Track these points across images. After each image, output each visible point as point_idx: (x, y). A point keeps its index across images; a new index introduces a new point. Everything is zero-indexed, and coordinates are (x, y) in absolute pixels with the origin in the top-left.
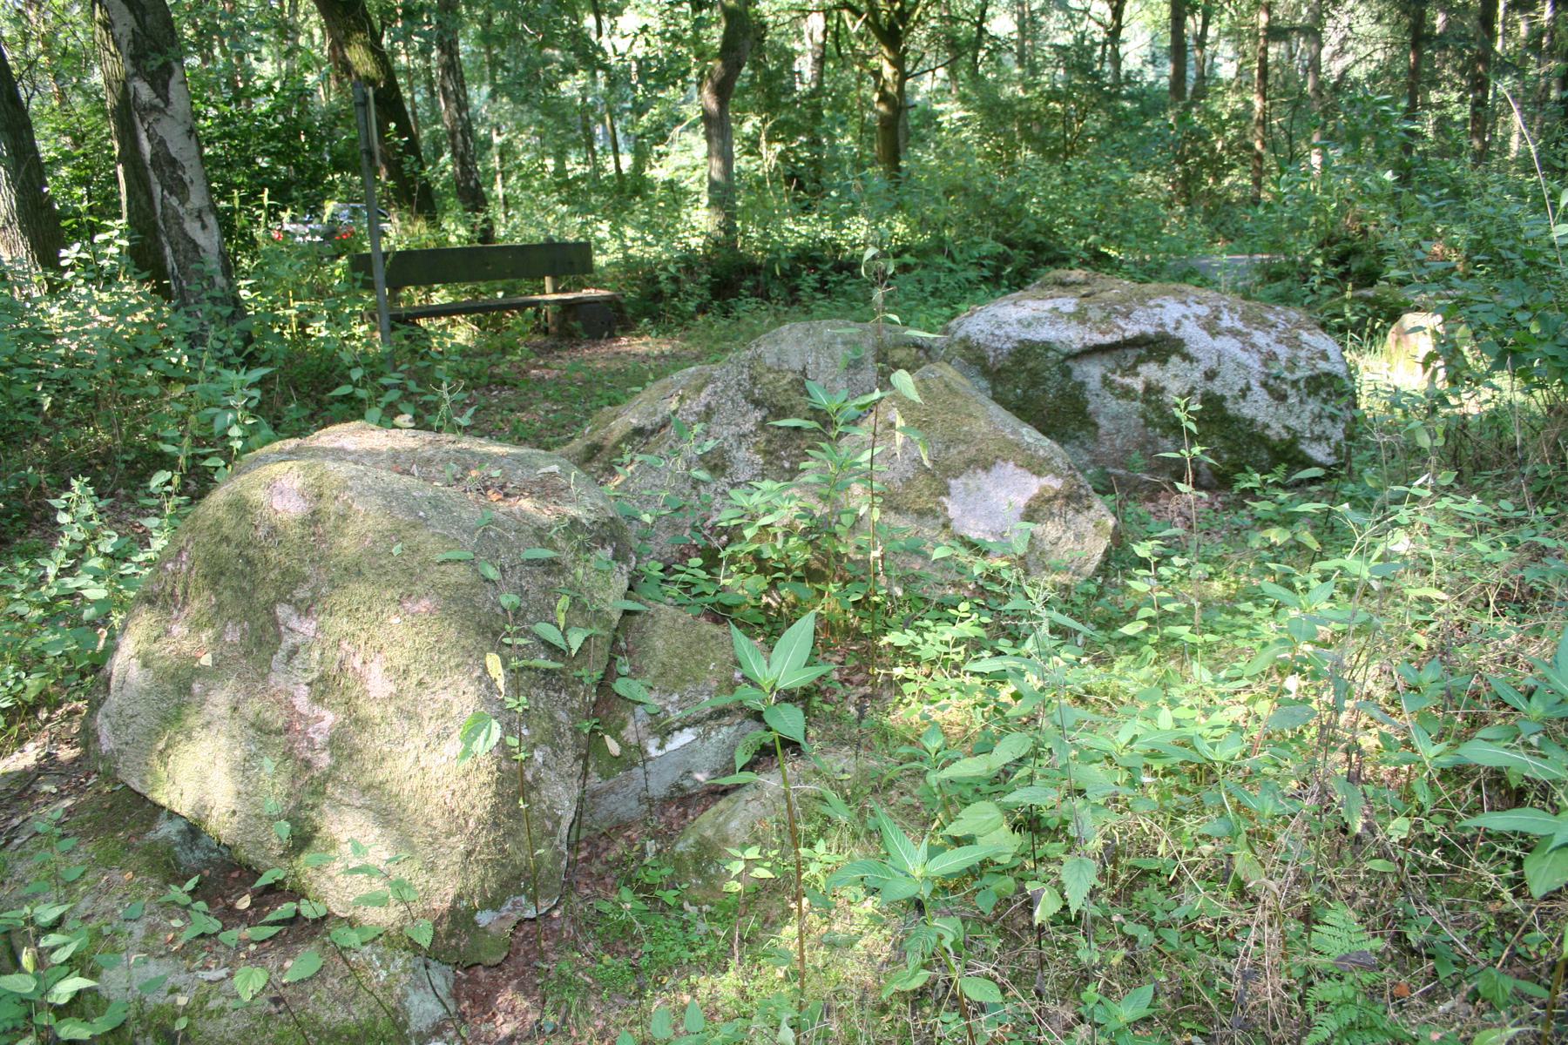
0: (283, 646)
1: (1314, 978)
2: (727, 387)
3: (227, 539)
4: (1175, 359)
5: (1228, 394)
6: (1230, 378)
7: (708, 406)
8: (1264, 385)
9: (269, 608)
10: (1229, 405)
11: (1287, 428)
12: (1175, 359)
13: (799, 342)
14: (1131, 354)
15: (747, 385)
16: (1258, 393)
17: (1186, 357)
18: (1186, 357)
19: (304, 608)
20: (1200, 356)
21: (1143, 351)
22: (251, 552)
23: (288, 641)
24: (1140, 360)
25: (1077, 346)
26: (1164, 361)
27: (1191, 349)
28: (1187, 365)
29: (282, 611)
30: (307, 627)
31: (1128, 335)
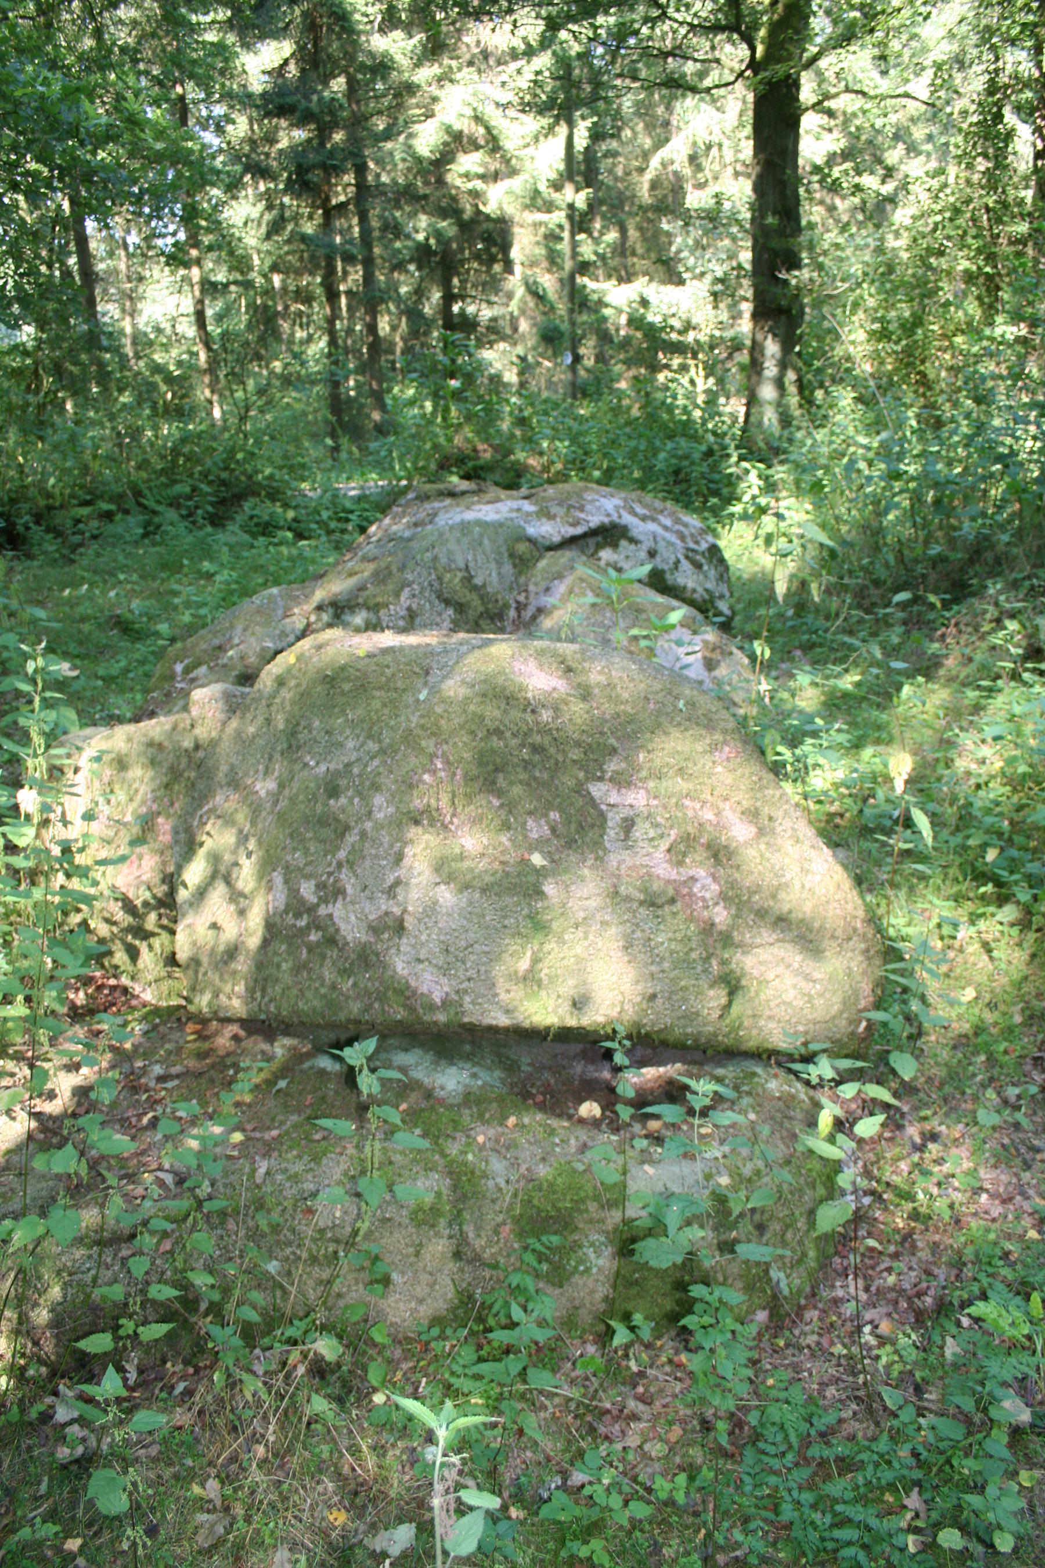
0: (610, 824)
1: (24, 1328)
2: (423, 589)
3: (498, 732)
4: (624, 543)
5: (666, 567)
6: (666, 554)
7: (409, 609)
8: (687, 557)
9: (580, 790)
10: (668, 576)
11: (706, 590)
12: (624, 543)
13: (458, 541)
14: (592, 542)
15: (436, 584)
16: (685, 565)
17: (632, 540)
18: (632, 540)
19: (622, 782)
20: (641, 537)
21: (600, 539)
22: (537, 739)
23: (614, 819)
24: (599, 547)
25: (557, 539)
26: (615, 546)
27: (634, 533)
28: (633, 547)
29: (597, 790)
30: (637, 798)
31: (592, 525)
